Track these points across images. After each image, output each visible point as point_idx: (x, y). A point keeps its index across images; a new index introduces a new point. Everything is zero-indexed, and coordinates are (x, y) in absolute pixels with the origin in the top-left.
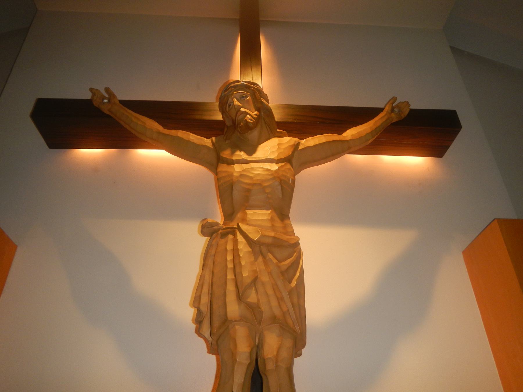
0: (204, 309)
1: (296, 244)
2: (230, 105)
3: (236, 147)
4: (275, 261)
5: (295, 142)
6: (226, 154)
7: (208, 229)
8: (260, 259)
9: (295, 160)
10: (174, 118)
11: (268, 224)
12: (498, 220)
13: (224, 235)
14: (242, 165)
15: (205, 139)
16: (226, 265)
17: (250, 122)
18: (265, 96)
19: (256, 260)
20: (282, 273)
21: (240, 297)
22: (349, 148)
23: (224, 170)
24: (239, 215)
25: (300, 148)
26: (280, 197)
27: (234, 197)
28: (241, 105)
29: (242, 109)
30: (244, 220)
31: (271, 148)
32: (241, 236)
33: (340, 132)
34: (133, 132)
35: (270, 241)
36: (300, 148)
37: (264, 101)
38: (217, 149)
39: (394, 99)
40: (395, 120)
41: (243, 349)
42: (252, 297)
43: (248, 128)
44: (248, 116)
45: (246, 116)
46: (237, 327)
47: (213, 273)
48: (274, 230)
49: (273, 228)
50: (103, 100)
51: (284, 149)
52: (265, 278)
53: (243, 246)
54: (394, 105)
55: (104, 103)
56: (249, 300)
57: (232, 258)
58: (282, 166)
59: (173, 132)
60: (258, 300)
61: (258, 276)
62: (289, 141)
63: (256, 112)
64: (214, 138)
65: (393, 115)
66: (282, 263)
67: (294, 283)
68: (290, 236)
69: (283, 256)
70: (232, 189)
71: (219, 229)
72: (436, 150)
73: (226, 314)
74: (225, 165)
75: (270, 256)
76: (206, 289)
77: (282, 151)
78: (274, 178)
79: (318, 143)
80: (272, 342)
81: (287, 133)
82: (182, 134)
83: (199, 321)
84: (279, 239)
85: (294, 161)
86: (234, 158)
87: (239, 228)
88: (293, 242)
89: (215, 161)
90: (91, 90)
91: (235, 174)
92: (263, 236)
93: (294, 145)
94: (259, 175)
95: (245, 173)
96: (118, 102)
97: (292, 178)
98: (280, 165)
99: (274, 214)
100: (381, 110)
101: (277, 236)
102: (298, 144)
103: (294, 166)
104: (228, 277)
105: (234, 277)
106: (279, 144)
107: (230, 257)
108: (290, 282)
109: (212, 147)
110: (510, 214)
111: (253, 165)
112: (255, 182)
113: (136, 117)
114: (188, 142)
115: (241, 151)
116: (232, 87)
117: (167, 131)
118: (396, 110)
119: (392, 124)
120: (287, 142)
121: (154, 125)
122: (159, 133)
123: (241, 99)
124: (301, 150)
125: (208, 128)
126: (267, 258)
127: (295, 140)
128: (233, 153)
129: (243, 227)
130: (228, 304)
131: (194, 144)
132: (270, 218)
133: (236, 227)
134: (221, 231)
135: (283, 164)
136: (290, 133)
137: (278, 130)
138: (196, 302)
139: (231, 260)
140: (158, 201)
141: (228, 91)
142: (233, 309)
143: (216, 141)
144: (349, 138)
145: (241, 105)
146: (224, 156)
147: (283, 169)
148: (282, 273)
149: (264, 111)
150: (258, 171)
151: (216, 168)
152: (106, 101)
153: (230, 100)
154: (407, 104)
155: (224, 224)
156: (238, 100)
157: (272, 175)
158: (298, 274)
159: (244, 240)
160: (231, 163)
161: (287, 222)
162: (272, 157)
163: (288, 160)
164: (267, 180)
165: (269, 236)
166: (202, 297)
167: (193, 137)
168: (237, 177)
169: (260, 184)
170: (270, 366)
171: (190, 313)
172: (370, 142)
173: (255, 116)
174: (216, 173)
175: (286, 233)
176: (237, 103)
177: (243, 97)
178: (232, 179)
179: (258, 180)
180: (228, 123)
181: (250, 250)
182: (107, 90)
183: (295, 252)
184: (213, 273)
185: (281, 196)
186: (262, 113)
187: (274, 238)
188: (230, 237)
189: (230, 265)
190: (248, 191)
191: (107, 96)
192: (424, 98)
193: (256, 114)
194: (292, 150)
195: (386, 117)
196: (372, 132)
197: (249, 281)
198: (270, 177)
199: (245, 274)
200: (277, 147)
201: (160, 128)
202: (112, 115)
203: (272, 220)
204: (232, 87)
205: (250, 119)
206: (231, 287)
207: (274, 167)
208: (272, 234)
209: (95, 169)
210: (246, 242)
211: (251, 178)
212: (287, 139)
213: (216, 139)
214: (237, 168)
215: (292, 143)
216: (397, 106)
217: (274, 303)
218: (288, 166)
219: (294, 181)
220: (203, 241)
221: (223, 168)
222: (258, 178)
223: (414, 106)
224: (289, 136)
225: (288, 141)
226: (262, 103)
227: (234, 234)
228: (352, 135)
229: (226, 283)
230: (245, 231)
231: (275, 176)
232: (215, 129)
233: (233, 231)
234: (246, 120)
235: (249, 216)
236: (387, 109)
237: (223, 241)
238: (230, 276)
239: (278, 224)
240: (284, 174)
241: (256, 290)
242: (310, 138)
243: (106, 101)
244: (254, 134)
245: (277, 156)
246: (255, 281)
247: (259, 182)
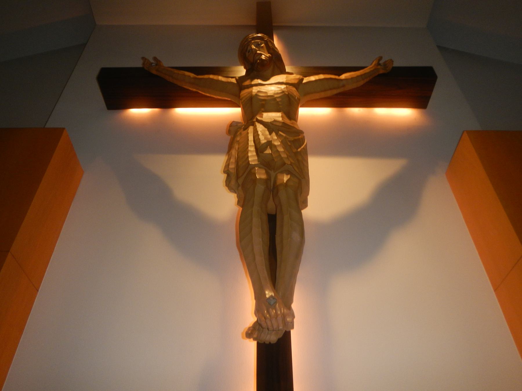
2: (249, 52)
12: (469, 132)
29: (258, 52)
39: (380, 58)
40: (381, 72)
72: (420, 101)
90: (143, 58)
102: (302, 80)
110: (476, 126)
119: (380, 76)
123: (258, 45)
124: (305, 83)
154: (392, 61)
160: (252, 86)
164: (278, 94)
182: (155, 59)
192: (406, 57)
195: (374, 68)
198: (280, 92)
207: (283, 87)
211: (266, 93)
214: (255, 90)
222: (271, 92)
223: (397, 64)
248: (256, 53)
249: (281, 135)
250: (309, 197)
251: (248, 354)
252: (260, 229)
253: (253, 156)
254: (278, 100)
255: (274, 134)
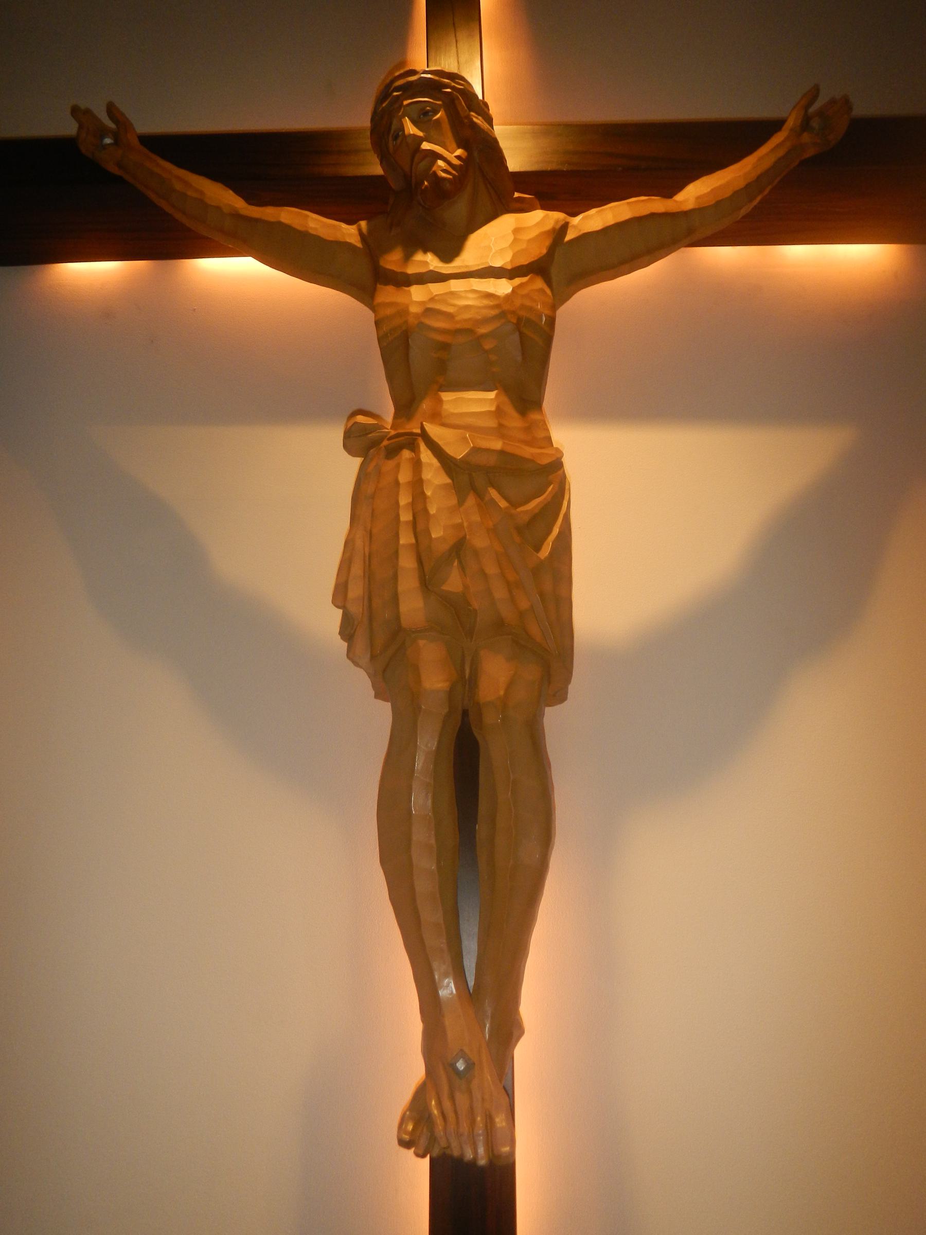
0: (356, 609)
1: (557, 465)
2: (396, 137)
3: (416, 243)
4: (503, 504)
5: (557, 221)
6: (392, 260)
7: (360, 440)
8: (471, 501)
9: (559, 268)
10: (270, 179)
11: (492, 423)
13: (393, 452)
14: (430, 285)
15: (343, 225)
16: (398, 516)
17: (444, 179)
18: (482, 108)
19: (461, 502)
20: (519, 530)
21: (427, 583)
22: (690, 231)
23: (388, 300)
24: (426, 405)
25: (568, 238)
26: (518, 357)
27: (417, 362)
28: (421, 134)
29: (426, 146)
30: (436, 416)
31: (500, 240)
32: (429, 452)
33: (669, 192)
34: (178, 216)
35: (492, 460)
36: (568, 238)
37: (478, 120)
38: (372, 248)
39: (814, 93)
40: (810, 152)
41: (435, 681)
42: (453, 582)
43: (442, 192)
44: (440, 163)
45: (434, 162)
46: (421, 643)
47: (371, 534)
48: (502, 436)
49: (500, 431)
50: (102, 137)
51: (529, 241)
52: (480, 541)
53: (434, 475)
54: (812, 110)
55: (105, 147)
56: (444, 588)
57: (410, 500)
58: (521, 285)
59: (269, 213)
60: (466, 587)
61: (464, 537)
62: (544, 217)
63: (459, 152)
64: (363, 224)
65: (806, 138)
66: (519, 509)
67: (545, 552)
68: (541, 448)
69: (524, 496)
70: (407, 347)
71: (381, 439)
73: (398, 617)
74: (390, 289)
75: (493, 493)
76: (357, 569)
77: (524, 246)
78: (503, 314)
79: (612, 222)
80: (496, 673)
81: (537, 203)
82: (289, 216)
83: (348, 631)
84: (513, 455)
85: (554, 271)
86: (411, 270)
87: (424, 435)
88: (545, 461)
89: (367, 277)
91: (414, 309)
92: (476, 450)
93: (554, 229)
94: (467, 307)
95: (437, 306)
96: (135, 142)
97: (547, 312)
98: (517, 281)
99: (504, 399)
100: (775, 125)
101: (509, 449)
102: (565, 227)
103: (554, 284)
104: (401, 542)
105: (413, 541)
106: (516, 231)
107: (404, 500)
108: (538, 549)
109: (359, 245)
111: (455, 285)
112: (458, 326)
113: (179, 178)
114: (305, 237)
115: (425, 252)
116: (397, 89)
117: (255, 212)
118: (815, 123)
120: (538, 224)
121: (226, 198)
122: (237, 216)
123: (422, 118)
125: (343, 197)
126: (487, 499)
127: (556, 217)
128: (408, 257)
129: (433, 430)
130: (402, 599)
131: (318, 239)
132: (493, 408)
133: (418, 431)
134: (385, 443)
135: (525, 279)
136: (547, 201)
137: (516, 195)
138: (340, 595)
139: (408, 504)
140: (245, 380)
141: (400, 92)
142: (413, 606)
143: (370, 231)
144: (690, 206)
145: (421, 134)
146: (388, 267)
147: (524, 291)
148: (519, 530)
149: (482, 150)
150: (467, 298)
151: (372, 297)
152: (108, 141)
153: (395, 122)
154: (846, 103)
155: (393, 426)
156: (415, 123)
157: (497, 306)
158: (556, 531)
159: (435, 462)
160: (405, 281)
161: (534, 416)
162: (498, 263)
163: (538, 268)
164: (486, 321)
165: (488, 450)
166: (350, 587)
167: (316, 223)
168: (417, 316)
169: (469, 331)
170: (491, 718)
171: (336, 616)
172: (743, 212)
173: (456, 162)
174: (373, 308)
175: (530, 443)
176: (411, 129)
177: (426, 113)
178: (406, 322)
179: (465, 320)
180: (395, 184)
181: (449, 481)
182: (111, 110)
183: (550, 483)
184: (371, 534)
185: (519, 359)
186: (476, 154)
187: (502, 452)
188: (406, 454)
189: (405, 516)
190: (445, 347)
191: (112, 126)
193: (458, 157)
194: (548, 242)
196: (748, 186)
197: (444, 547)
199: (436, 533)
200: (511, 238)
201: (238, 203)
202: (127, 177)
203: (499, 412)
204: (397, 89)
205: (445, 171)
206: (407, 562)
207: (503, 287)
208: (497, 445)
209: (106, 310)
210: (438, 464)
211: (449, 316)
212: (538, 215)
213: (368, 224)
214: (418, 294)
215: (549, 225)
216: (820, 113)
217: (500, 593)
218: (539, 283)
219: (552, 321)
220: (354, 463)
221: (387, 295)
222: (467, 316)
223: (861, 109)
224: (544, 208)
225: (539, 220)
226: (474, 126)
227: (413, 447)
228: (698, 198)
229: (396, 553)
230: (436, 439)
231: (503, 310)
232: (377, 193)
233: (410, 442)
234: (435, 173)
235: (446, 407)
236: (790, 123)
237: (391, 464)
238: (406, 539)
239: (514, 421)
240: (528, 303)
241: (462, 568)
242: (593, 211)
243: (108, 141)
244: (459, 209)
245: (511, 261)
246: (459, 548)
247: (466, 326)
248: (418, 149)
249: (492, 500)
250: (570, 686)
251: (412, 1181)
252: (430, 802)
253: (479, 1135)
254: (488, 345)
255: (471, 501)
